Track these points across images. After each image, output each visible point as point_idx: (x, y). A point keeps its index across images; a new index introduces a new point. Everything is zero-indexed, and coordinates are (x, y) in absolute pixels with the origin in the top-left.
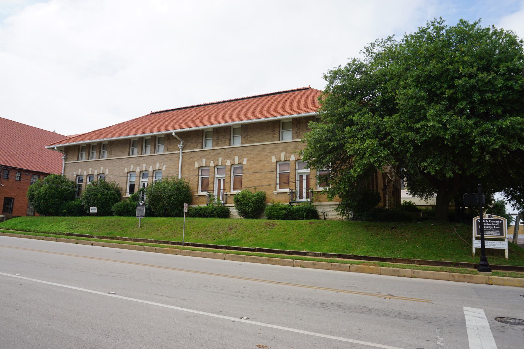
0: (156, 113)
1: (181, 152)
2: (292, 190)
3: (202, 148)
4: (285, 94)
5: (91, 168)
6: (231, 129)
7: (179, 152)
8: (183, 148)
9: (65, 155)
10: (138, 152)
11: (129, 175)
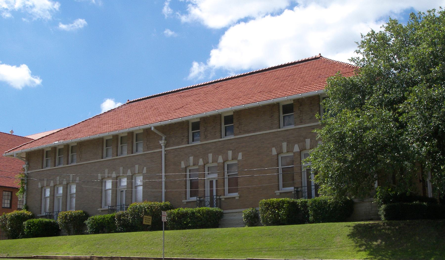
0: (256, 72)
1: (163, 150)
2: (297, 188)
3: (188, 144)
4: (267, 72)
5: (59, 177)
6: (279, 107)
7: (161, 150)
8: (166, 144)
9: (26, 163)
10: (113, 153)
11: (56, 188)
